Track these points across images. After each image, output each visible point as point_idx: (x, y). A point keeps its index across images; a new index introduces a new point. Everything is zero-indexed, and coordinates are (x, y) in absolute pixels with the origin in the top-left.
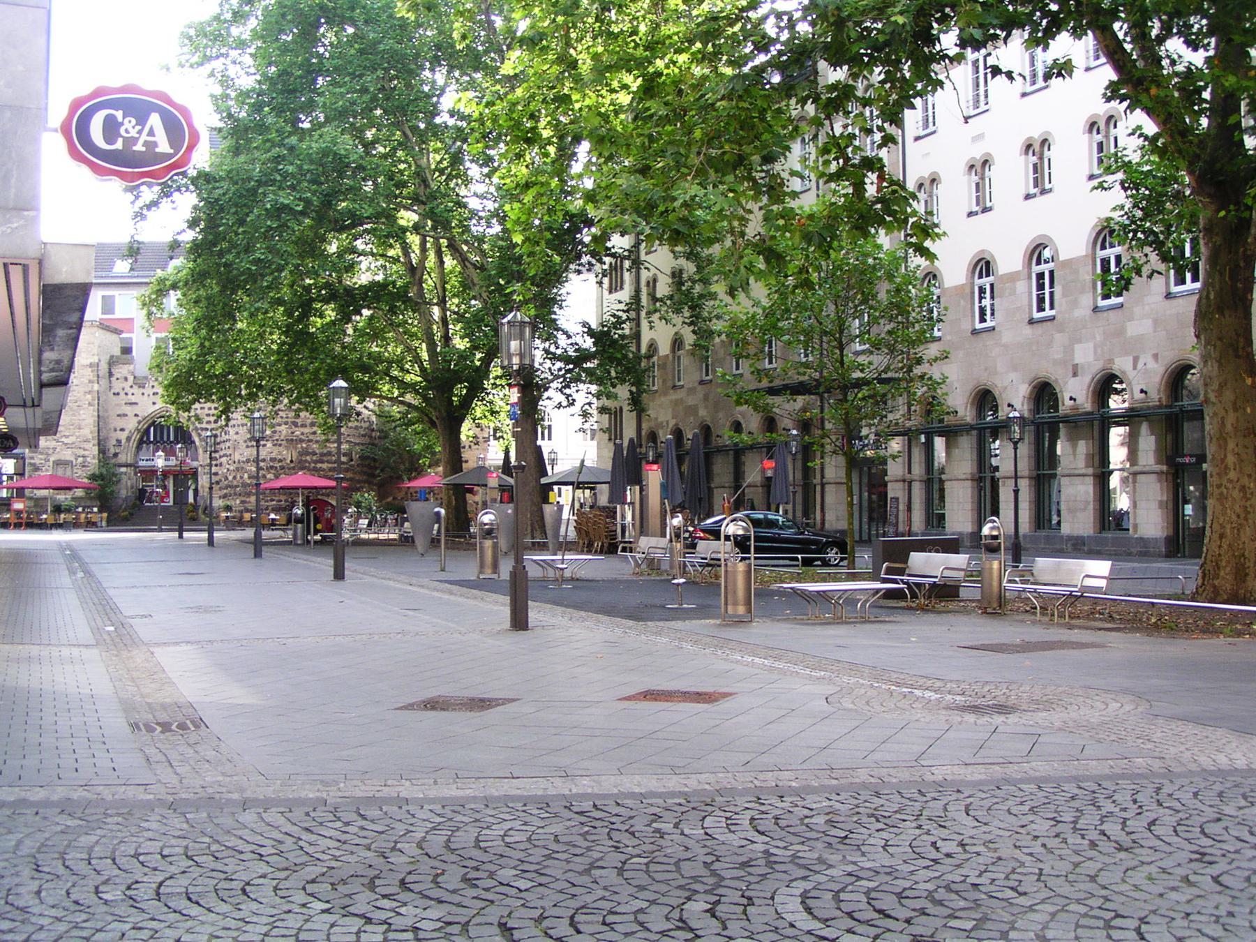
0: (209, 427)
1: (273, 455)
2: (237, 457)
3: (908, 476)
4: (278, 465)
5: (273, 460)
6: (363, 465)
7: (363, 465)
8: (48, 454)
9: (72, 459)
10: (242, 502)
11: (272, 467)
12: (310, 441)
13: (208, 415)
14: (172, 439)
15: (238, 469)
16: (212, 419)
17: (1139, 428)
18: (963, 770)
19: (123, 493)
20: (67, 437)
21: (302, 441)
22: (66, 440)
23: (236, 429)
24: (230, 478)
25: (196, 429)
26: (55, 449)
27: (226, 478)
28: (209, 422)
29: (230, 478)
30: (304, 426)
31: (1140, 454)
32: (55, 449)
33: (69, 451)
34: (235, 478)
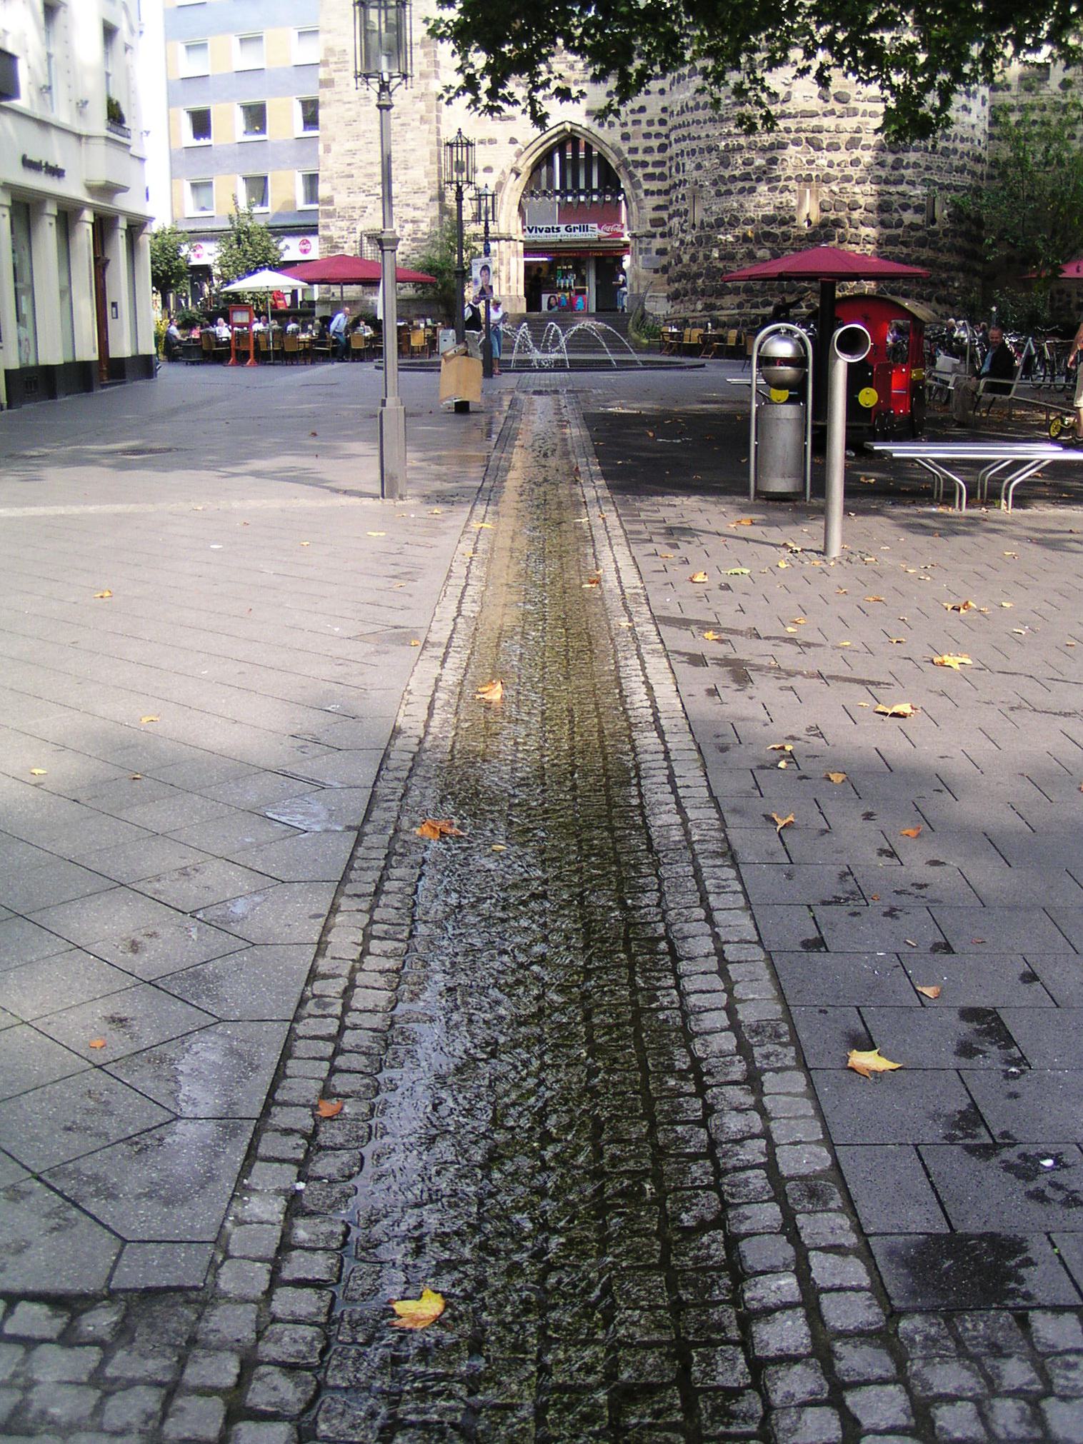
0: (649, 158)
2: (698, 215)
6: (955, 234)
7: (955, 234)
8: (352, 219)
10: (709, 307)
12: (847, 179)
13: (647, 136)
14: (595, 186)
15: (699, 241)
18: (699, 521)
21: (827, 180)
23: (697, 159)
24: (686, 258)
25: (625, 164)
27: (679, 260)
28: (648, 150)
29: (686, 258)
30: (834, 147)
31: (152, 1283)
34: (694, 258)
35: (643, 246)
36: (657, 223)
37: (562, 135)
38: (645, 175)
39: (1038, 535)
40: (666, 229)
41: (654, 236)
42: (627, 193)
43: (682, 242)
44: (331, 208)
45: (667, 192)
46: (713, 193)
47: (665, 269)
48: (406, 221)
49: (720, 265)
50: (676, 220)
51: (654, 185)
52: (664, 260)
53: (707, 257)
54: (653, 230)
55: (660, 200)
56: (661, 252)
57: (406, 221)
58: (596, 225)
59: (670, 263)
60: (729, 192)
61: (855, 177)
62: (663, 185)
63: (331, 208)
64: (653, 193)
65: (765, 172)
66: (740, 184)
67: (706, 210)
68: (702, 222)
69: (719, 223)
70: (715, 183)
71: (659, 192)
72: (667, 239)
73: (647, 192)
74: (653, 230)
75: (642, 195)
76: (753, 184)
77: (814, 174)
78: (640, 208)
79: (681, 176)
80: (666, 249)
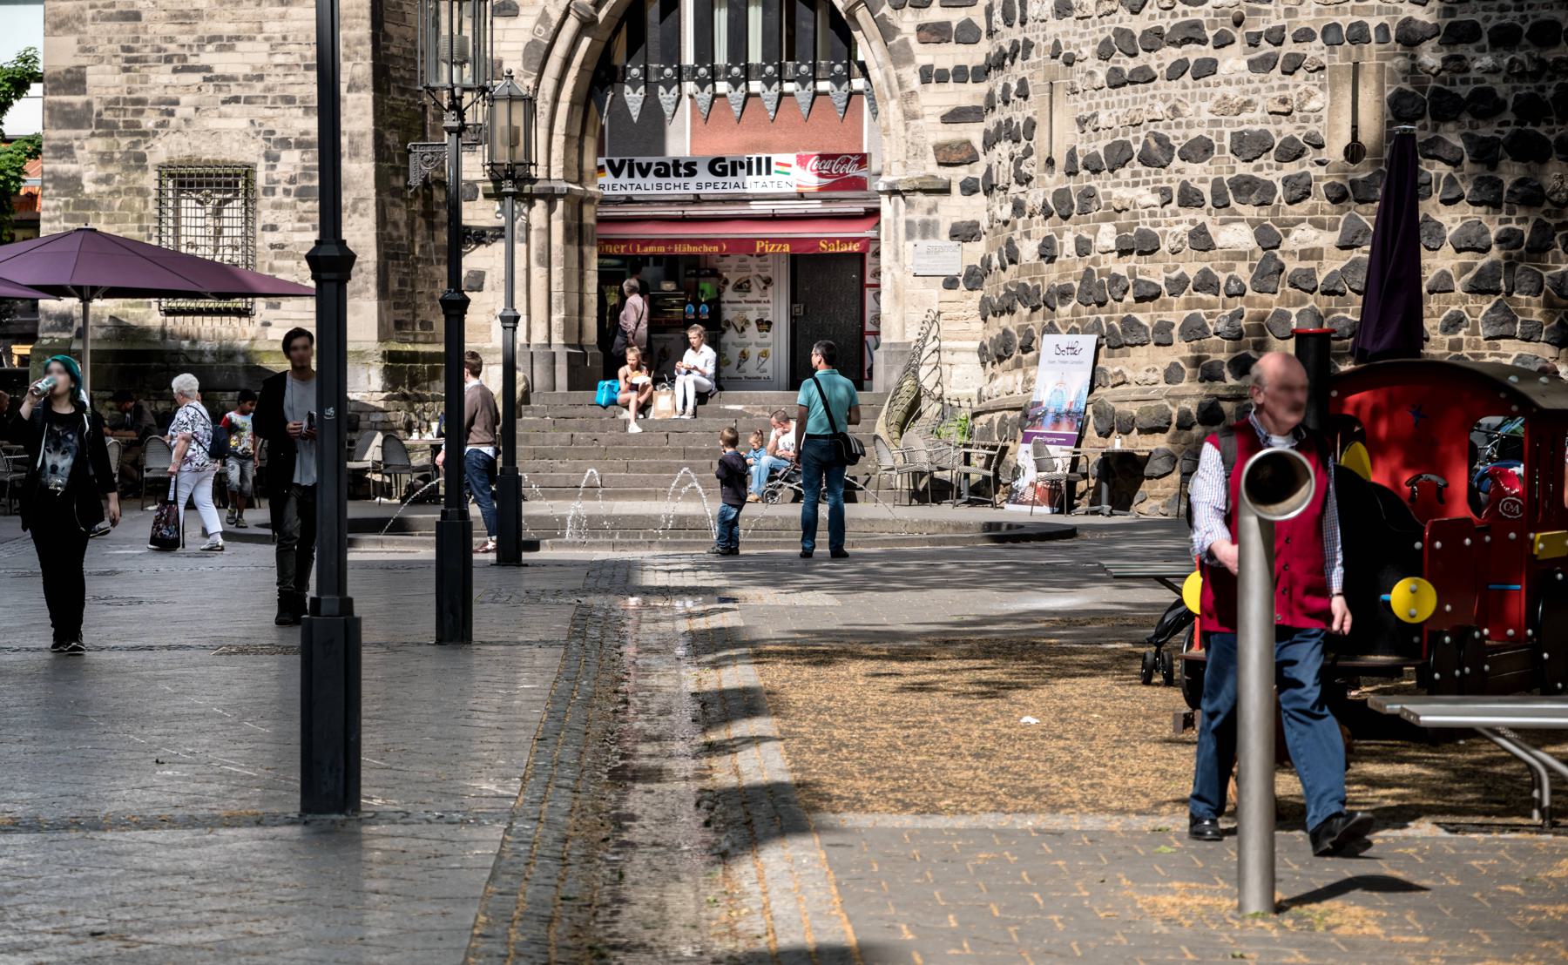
1: (1253, 120)
4: (1272, 172)
5: (1250, 145)
9: (251, 152)
11: (1246, 188)
17: (622, 90)
20: (225, 44)
22: (222, 63)
24: (1028, 250)
26: (168, 106)
27: (1012, 256)
29: (1028, 250)
33: (237, 120)
34: (1048, 253)
35: (918, 216)
36: (950, 156)
37: (866, 376)
38: (920, 28)
39: (984, 689)
40: (978, 171)
41: (945, 190)
42: (875, 74)
43: (1018, 208)
44: (77, 100)
45: (980, 74)
46: (1101, 78)
47: (974, 278)
48: (285, 143)
49: (1121, 267)
50: (1004, 148)
51: (947, 56)
52: (974, 252)
53: (1083, 247)
54: (945, 173)
55: (969, 94)
56: (965, 233)
57: (285, 143)
58: (791, 158)
59: (986, 262)
60: (1145, 77)
61: (1486, 27)
62: (975, 55)
63: (77, 100)
64: (942, 77)
65: (1238, 23)
66: (1170, 55)
67: (1082, 122)
68: (1072, 155)
69: (1118, 156)
70: (1104, 52)
71: (960, 74)
72: (980, 198)
73: (927, 75)
74: (945, 173)
75: (914, 82)
76: (1207, 51)
77: (1373, 22)
78: (910, 116)
79: (1016, 33)
80: (976, 224)
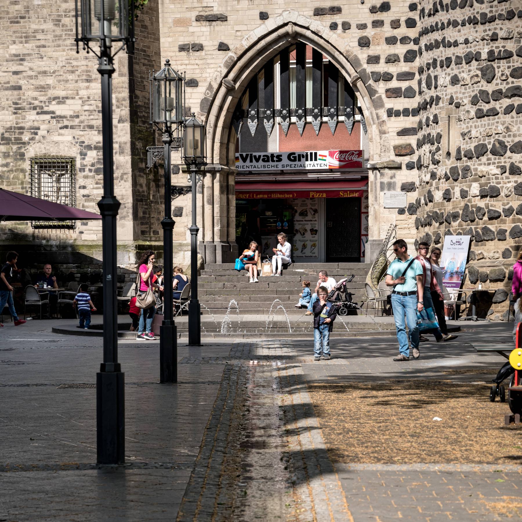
0: (394, 69)
3: (120, 101)
9: (73, 152)
16: (400, 50)
19: (267, 401)
20: (61, 100)
24: (438, 196)
26: (35, 130)
28: (392, 60)
29: (438, 196)
32: (35, 130)
33: (67, 136)
34: (447, 197)
